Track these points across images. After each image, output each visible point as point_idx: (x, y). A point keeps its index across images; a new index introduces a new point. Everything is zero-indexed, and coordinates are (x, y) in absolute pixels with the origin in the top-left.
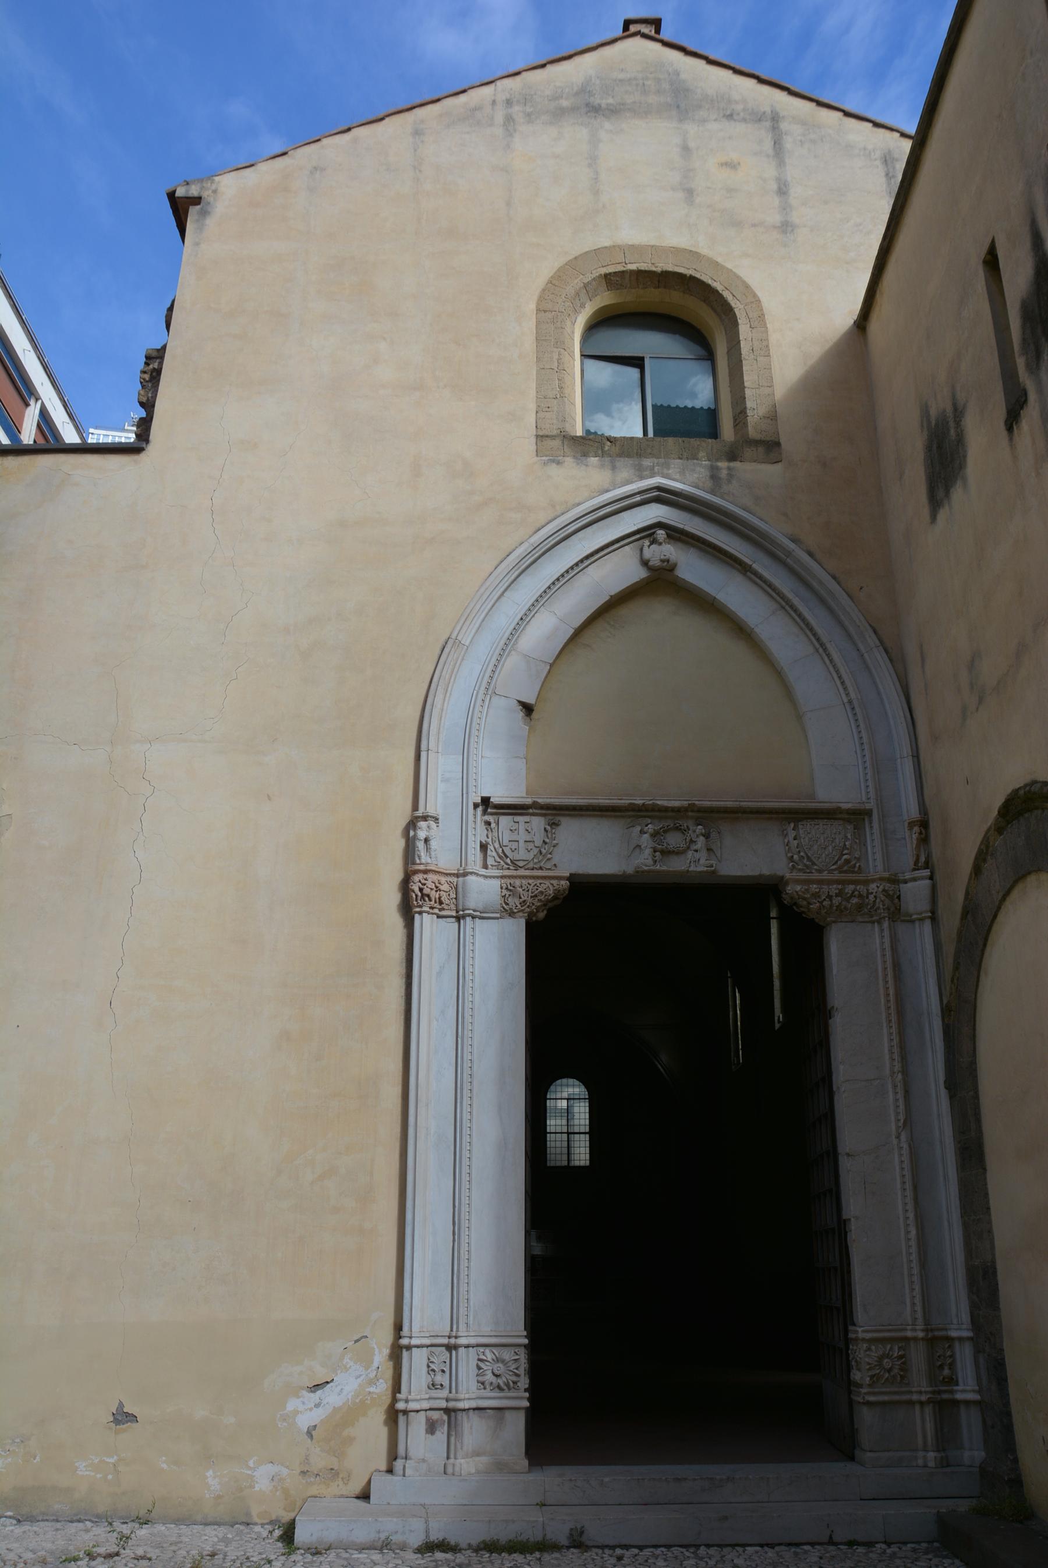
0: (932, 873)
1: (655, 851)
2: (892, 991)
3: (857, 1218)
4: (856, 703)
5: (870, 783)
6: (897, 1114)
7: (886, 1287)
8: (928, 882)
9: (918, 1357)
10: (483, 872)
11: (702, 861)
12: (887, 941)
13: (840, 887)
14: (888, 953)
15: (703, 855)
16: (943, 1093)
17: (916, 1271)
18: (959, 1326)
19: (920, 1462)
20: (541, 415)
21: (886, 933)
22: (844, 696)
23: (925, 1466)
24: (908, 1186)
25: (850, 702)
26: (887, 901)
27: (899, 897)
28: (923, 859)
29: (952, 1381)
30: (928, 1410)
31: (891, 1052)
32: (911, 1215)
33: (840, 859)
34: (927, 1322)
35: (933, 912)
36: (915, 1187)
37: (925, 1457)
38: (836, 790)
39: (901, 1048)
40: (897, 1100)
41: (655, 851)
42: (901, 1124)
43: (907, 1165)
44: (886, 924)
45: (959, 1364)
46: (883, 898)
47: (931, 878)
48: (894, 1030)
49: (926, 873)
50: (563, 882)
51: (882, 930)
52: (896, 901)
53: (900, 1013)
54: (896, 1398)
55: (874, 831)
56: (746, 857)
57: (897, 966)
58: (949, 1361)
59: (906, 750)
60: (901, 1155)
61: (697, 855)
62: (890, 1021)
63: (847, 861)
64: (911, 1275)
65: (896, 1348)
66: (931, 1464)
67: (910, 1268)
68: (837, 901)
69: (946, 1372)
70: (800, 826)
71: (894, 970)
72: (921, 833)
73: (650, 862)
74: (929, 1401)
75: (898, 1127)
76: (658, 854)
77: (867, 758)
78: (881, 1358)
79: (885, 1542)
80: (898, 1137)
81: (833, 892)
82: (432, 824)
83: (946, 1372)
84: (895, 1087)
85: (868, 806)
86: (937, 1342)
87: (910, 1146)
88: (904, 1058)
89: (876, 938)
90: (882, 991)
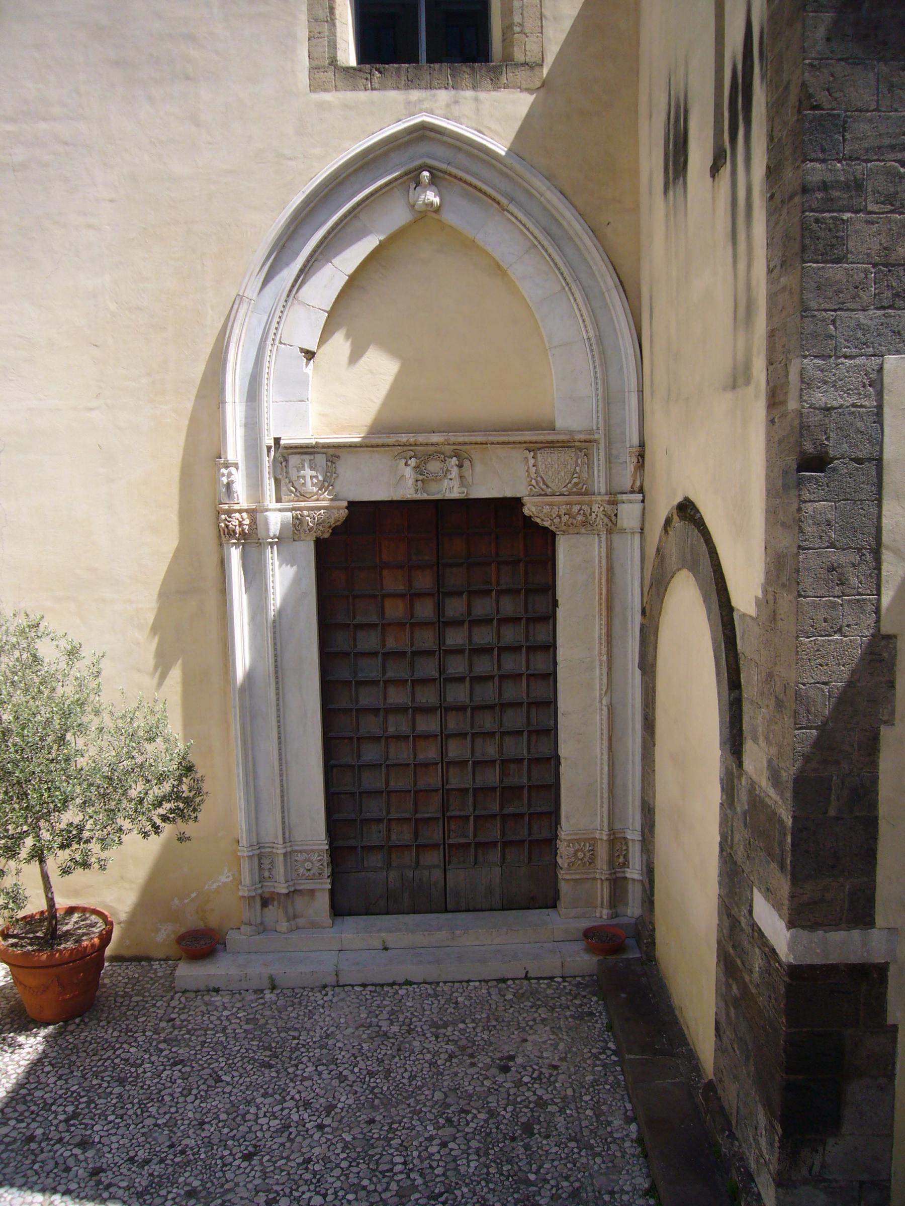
0: (644, 496)
1: (417, 481)
2: (604, 591)
3: (565, 759)
4: (593, 341)
5: (600, 414)
6: (601, 685)
7: (580, 812)
8: (640, 505)
9: (602, 852)
10: (279, 505)
11: (455, 489)
12: (604, 550)
13: (568, 506)
14: (604, 562)
15: (456, 483)
16: (638, 672)
17: (606, 795)
18: (633, 835)
19: (598, 915)
20: (315, 41)
21: (604, 545)
22: (584, 332)
23: (601, 917)
24: (605, 737)
25: (589, 339)
26: (606, 520)
27: (616, 515)
28: (638, 484)
29: (626, 864)
30: (606, 884)
31: (600, 638)
32: (605, 757)
33: (570, 482)
34: (611, 829)
35: (642, 529)
36: (610, 739)
37: (601, 912)
38: (572, 418)
39: (608, 636)
40: (601, 674)
41: (417, 481)
42: (603, 692)
43: (605, 722)
44: (604, 538)
45: (630, 854)
46: (602, 516)
47: (643, 501)
48: (603, 622)
49: (640, 497)
50: (341, 511)
51: (600, 542)
52: (614, 518)
53: (610, 608)
54: (585, 876)
55: (600, 462)
56: (492, 480)
57: (610, 570)
58: (624, 853)
59: (634, 386)
60: (601, 714)
61: (451, 484)
62: (601, 615)
63: (576, 484)
64: (602, 797)
65: (588, 845)
66: (605, 917)
67: (602, 793)
68: (565, 519)
69: (621, 860)
70: (539, 455)
71: (607, 575)
72: (638, 462)
73: (412, 491)
74: (607, 879)
75: (601, 694)
76: (419, 483)
77: (600, 392)
78: (576, 852)
79: (562, 977)
80: (601, 702)
81: (562, 512)
82: (233, 469)
83: (621, 860)
84: (601, 665)
85: (596, 437)
86: (616, 841)
87: (608, 709)
88: (609, 643)
89: (596, 547)
90: (597, 590)
